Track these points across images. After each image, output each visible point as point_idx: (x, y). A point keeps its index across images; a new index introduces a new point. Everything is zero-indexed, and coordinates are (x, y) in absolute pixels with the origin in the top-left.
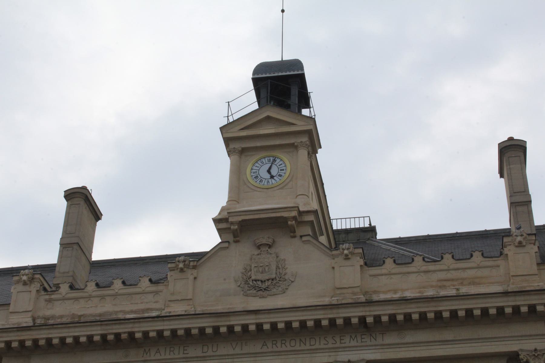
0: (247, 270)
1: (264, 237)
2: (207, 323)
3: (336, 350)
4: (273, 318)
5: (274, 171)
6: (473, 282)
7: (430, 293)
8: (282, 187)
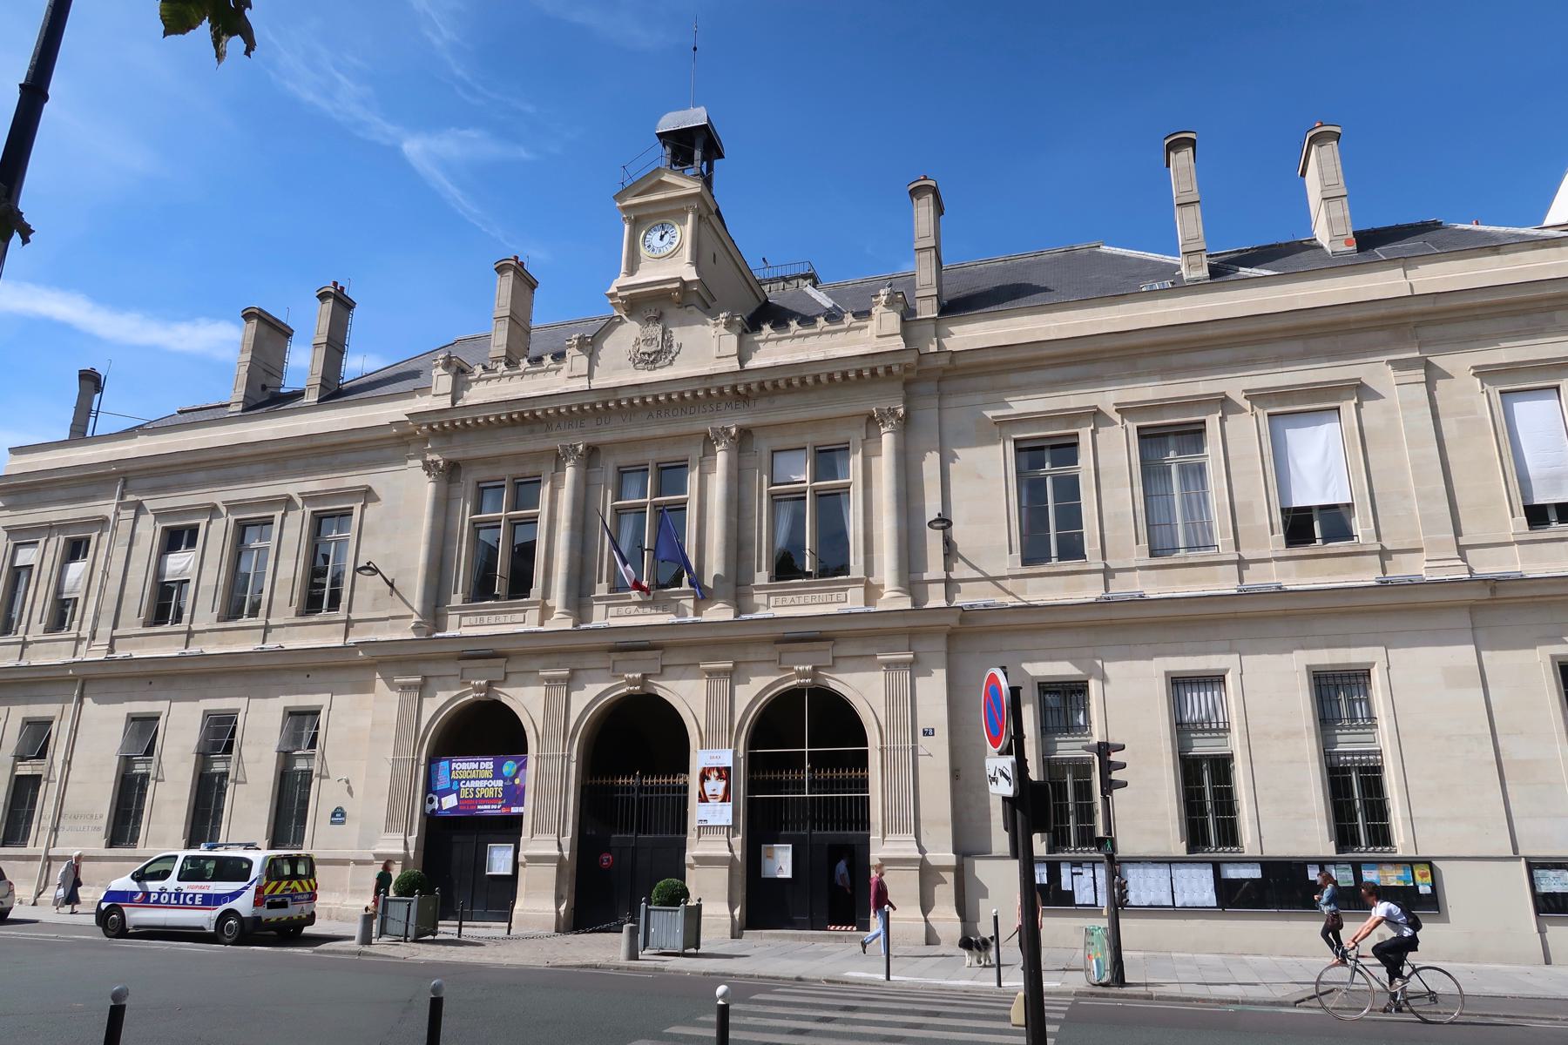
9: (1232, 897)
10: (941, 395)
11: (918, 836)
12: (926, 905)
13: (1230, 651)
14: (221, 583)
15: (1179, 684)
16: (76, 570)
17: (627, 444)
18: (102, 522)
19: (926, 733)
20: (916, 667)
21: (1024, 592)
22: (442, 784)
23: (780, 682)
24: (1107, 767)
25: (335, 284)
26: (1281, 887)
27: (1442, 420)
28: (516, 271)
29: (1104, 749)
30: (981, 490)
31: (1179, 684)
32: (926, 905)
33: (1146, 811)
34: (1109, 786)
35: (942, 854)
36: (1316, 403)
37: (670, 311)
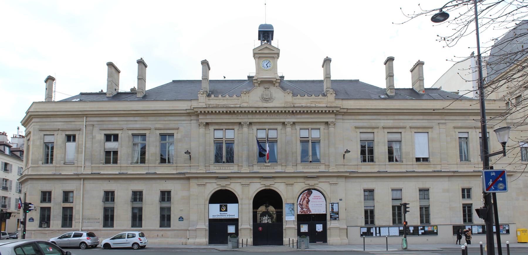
0: (262, 95)
1: (267, 86)
2: (254, 110)
3: (285, 118)
4: (333, 109)
5: (268, 65)
6: (319, 103)
7: (308, 105)
8: (270, 70)
24: (406, 208)
29: (405, 205)
34: (406, 212)
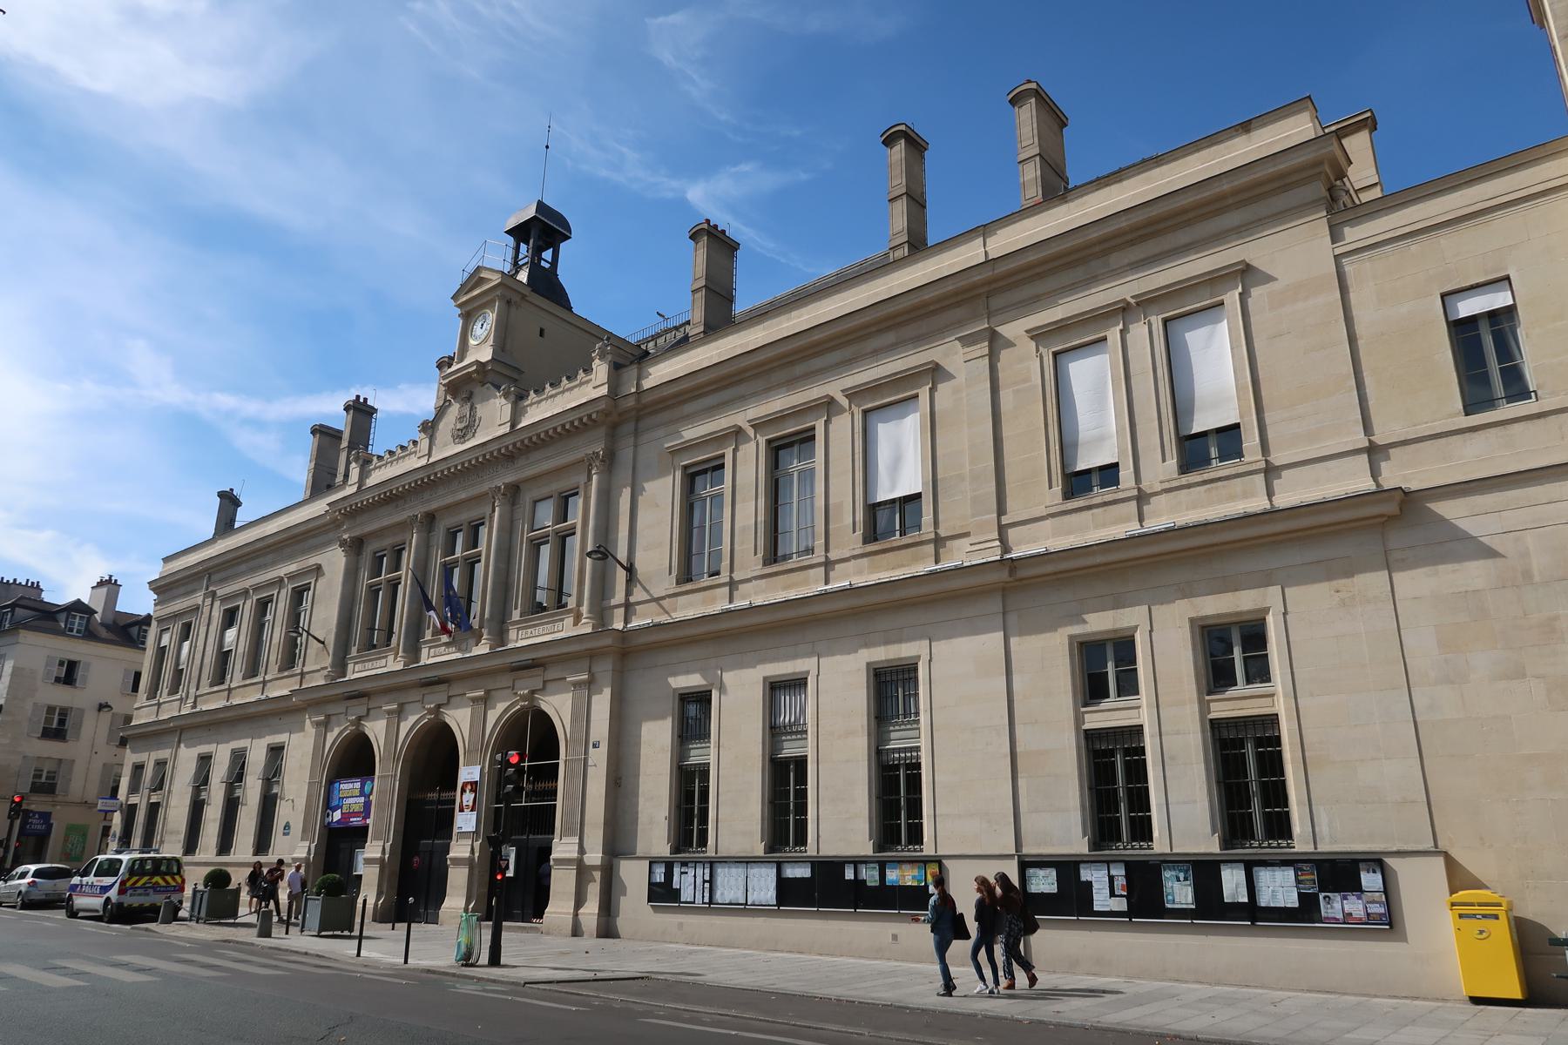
9: (789, 894)
10: (637, 433)
11: (581, 839)
12: (579, 902)
13: (809, 655)
14: (761, 518)
15: (775, 688)
16: (231, 634)
17: (448, 507)
18: (196, 609)
19: (595, 746)
20: (591, 685)
21: (675, 610)
22: (335, 803)
23: (506, 711)
25: (708, 221)
26: (827, 889)
27: (1002, 393)
28: (709, 233)
30: (654, 513)
31: (775, 688)
32: (579, 902)
33: (738, 814)
35: (594, 857)
36: (1180, 308)
37: (478, 390)
